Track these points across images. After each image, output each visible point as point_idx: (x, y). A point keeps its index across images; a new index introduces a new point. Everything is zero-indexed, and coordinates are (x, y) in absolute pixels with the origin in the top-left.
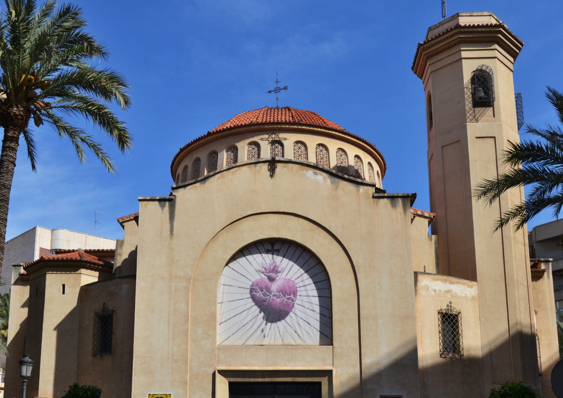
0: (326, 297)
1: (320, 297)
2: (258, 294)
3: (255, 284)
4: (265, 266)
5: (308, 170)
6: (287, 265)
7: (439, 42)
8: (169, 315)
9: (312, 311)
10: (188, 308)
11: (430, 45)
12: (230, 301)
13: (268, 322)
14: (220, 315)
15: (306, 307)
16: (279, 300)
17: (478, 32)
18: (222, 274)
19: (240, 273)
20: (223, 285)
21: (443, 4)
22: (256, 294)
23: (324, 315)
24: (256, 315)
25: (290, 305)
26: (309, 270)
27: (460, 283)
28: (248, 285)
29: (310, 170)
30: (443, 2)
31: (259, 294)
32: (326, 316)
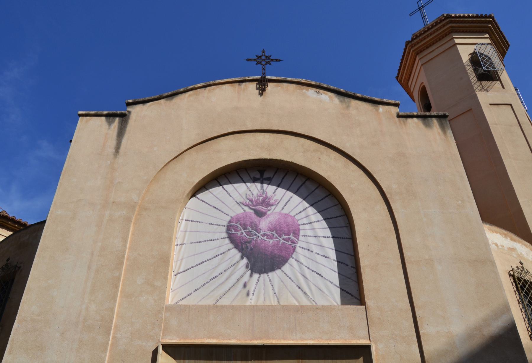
0: (345, 238)
1: (336, 238)
2: (239, 233)
3: (235, 219)
4: (251, 197)
5: (309, 89)
6: (283, 196)
7: (428, 36)
8: (92, 254)
9: (324, 258)
10: (125, 246)
11: (419, 40)
12: (195, 243)
13: (254, 273)
14: (177, 261)
15: (314, 251)
16: (271, 241)
17: (468, 22)
18: (186, 207)
19: (213, 205)
20: (186, 220)
21: (423, 18)
22: (235, 232)
23: (344, 264)
24: (235, 262)
25: (289, 248)
26: (316, 203)
27: (521, 242)
28: (225, 220)
29: (311, 90)
30: (423, 17)
31: (241, 233)
32: (347, 265)
